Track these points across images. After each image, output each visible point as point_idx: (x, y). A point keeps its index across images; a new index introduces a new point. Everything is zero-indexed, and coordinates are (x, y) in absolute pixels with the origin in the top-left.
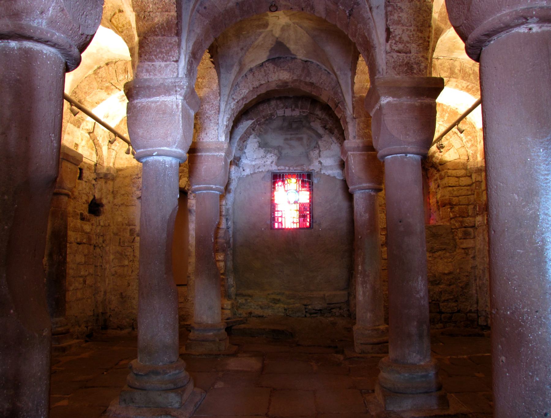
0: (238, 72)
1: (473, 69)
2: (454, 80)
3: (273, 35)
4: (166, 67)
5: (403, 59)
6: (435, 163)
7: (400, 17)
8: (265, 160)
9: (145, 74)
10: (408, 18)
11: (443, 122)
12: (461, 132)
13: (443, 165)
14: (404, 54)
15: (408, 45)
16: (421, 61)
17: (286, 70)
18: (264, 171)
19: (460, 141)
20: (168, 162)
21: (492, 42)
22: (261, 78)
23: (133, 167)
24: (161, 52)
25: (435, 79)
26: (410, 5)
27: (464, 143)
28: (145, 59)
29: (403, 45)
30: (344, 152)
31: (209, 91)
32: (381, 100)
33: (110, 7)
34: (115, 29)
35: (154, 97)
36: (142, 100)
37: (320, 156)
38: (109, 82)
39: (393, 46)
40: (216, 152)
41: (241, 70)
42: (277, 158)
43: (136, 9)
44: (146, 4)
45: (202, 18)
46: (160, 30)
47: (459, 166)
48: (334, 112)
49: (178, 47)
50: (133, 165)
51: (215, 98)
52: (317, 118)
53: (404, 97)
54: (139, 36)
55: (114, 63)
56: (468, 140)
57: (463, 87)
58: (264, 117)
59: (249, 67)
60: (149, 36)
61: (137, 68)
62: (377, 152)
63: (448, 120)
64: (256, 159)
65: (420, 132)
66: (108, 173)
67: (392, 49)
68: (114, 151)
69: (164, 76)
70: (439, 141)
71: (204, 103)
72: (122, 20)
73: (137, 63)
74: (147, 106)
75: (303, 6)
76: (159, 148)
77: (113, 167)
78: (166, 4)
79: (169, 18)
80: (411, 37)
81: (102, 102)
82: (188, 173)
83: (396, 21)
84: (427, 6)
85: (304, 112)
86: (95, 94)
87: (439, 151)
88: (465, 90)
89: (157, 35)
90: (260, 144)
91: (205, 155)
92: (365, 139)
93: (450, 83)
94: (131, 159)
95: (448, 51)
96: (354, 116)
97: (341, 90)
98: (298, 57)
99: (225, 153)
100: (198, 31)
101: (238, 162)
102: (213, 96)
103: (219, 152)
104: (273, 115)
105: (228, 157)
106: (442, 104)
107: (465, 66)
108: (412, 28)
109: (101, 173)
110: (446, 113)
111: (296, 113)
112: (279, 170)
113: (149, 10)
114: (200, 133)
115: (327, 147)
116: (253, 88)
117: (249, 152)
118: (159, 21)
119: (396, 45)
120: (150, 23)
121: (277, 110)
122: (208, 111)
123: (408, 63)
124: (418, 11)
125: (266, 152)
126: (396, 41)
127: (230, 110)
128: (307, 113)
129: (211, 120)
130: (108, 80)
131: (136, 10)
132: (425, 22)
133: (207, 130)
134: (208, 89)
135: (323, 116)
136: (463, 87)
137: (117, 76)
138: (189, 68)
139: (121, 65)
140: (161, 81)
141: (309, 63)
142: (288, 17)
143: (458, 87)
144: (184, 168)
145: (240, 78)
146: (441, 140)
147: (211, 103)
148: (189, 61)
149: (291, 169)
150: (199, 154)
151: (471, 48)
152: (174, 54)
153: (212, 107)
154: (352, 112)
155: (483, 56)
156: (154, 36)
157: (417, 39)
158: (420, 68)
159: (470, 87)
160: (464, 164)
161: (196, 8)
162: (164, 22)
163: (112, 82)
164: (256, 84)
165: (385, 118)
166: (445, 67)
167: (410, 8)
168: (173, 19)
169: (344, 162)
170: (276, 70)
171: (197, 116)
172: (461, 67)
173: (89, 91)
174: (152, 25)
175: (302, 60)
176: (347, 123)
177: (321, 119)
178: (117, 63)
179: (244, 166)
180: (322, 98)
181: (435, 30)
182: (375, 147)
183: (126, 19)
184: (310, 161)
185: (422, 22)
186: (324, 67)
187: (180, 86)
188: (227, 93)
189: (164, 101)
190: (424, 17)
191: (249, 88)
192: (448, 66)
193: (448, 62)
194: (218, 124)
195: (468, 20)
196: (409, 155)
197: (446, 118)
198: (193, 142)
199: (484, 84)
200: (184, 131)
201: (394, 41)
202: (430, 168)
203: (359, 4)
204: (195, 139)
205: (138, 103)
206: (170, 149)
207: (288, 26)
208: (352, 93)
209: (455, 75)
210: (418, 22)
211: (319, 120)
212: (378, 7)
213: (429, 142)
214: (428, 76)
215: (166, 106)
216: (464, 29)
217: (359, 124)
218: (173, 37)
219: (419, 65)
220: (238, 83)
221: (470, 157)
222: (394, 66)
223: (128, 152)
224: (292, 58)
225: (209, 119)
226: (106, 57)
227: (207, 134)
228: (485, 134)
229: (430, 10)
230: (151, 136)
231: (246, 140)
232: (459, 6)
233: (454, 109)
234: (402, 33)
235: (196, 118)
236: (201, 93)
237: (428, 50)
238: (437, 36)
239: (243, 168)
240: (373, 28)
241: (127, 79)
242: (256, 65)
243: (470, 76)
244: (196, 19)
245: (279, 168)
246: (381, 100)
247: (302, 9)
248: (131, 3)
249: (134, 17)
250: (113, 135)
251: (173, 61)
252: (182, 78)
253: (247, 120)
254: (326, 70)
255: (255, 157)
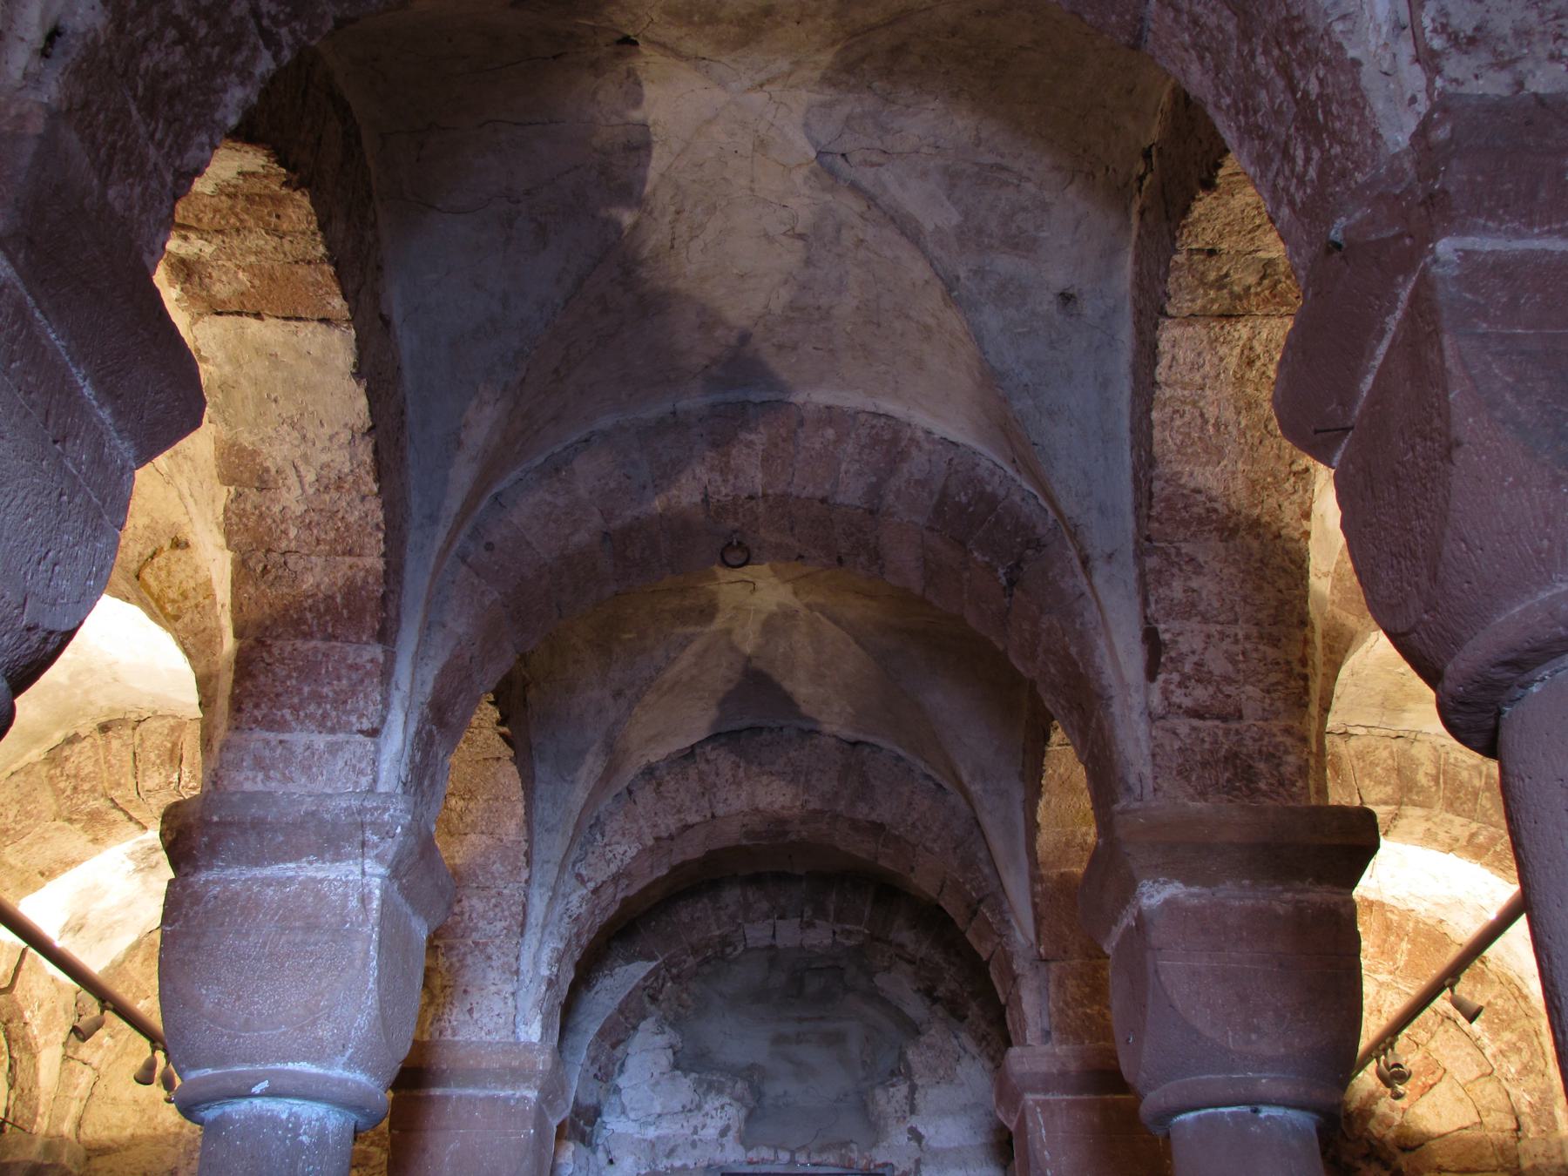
0: (601, 779)
1: (1485, 773)
2: (1419, 812)
3: (733, 648)
4: (330, 752)
5: (1216, 742)
6: (1381, 1140)
7: (1194, 591)
8: (696, 1120)
9: (250, 774)
10: (1224, 593)
11: (1391, 973)
12: (1472, 1016)
13: (1412, 1149)
14: (1217, 723)
15: (1228, 689)
16: (1282, 748)
17: (781, 775)
18: (692, 1166)
19: (1470, 1050)
20: (310, 1123)
21: (1535, 689)
22: (688, 803)
23: (156, 1140)
24: (318, 698)
25: (1342, 811)
26: (1227, 549)
27: (1492, 1062)
28: (256, 721)
29: (1211, 690)
30: (1007, 1091)
31: (488, 846)
32: (1143, 894)
33: (140, 526)
34: (153, 604)
35: (277, 863)
36: (230, 871)
37: (913, 1110)
38: (104, 795)
39: (1172, 692)
40: (504, 1084)
41: (611, 771)
42: (743, 1113)
43: (236, 539)
44: (274, 526)
45: (476, 582)
46: (320, 616)
47: (1482, 1157)
48: (963, 934)
49: (381, 683)
50: (160, 1131)
51: (511, 872)
52: (901, 958)
53: (1228, 883)
54: (238, 634)
55: (131, 725)
56: (1504, 1047)
57: (1457, 840)
58: (695, 951)
59: (644, 762)
60: (278, 637)
61: (221, 750)
62: (1139, 1098)
63: (1412, 969)
64: (659, 1116)
65: (1302, 1016)
66: (46, 1162)
67: (1169, 704)
68: (88, 1070)
69: (319, 786)
70: (1385, 1051)
71: (468, 892)
72: (183, 576)
73: (221, 733)
74: (244, 895)
75: (843, 551)
76: (279, 1066)
77: (73, 1138)
78: (347, 528)
79: (354, 576)
80: (1239, 662)
81: (64, 871)
82: (384, 1168)
83: (1180, 603)
84: (1287, 552)
85: (848, 934)
86: (43, 838)
87: (1389, 1091)
88: (1464, 848)
89: (308, 636)
90: (679, 1055)
91: (460, 1098)
92: (1087, 1042)
93: (1402, 823)
94: (155, 1103)
95: (1382, 705)
96: (1042, 951)
97: (988, 849)
98: (828, 728)
99: (541, 1090)
100: (459, 625)
101: (588, 1129)
102: (502, 865)
103: (514, 1085)
104: (730, 944)
105: (550, 1104)
106: (1382, 905)
107: (1452, 761)
108: (1240, 631)
109: (17, 1163)
110: (1402, 940)
111: (820, 937)
112: (750, 1163)
113: (284, 545)
114: (444, 1006)
115: (941, 1072)
116: (657, 839)
117: (632, 1087)
118: (318, 586)
119: (1183, 691)
120: (285, 590)
121: (746, 925)
122: (482, 924)
123: (1232, 757)
124: (1256, 569)
125: (700, 1091)
126: (1183, 675)
127: (567, 920)
128: (861, 938)
129: (489, 958)
130: (100, 788)
131: (237, 545)
132: (1287, 607)
133: (475, 997)
134: (484, 837)
135: (924, 950)
136: (1457, 840)
137: (140, 773)
138: (418, 759)
139: (156, 736)
140: (308, 805)
141: (867, 750)
142: (789, 587)
143: (1436, 840)
144: (373, 1149)
145: (609, 801)
146: (1391, 1045)
147: (494, 892)
148: (418, 733)
149: (801, 1158)
150: (437, 1092)
151: (1461, 708)
152: (366, 708)
153: (495, 906)
154: (1032, 936)
155: (1508, 736)
156: (296, 637)
157: (1262, 669)
158: (1280, 774)
159: (1481, 839)
160: (1502, 1149)
161: (457, 545)
162: (335, 588)
163: (114, 794)
164: (668, 827)
165: (1159, 963)
166: (1377, 765)
167: (1226, 561)
168: (371, 579)
169: (1010, 1133)
170: (741, 773)
171: (437, 942)
172: (1436, 763)
173: (19, 827)
174: (290, 598)
175: (841, 740)
176: (1015, 978)
177: (914, 963)
178: (143, 725)
179: (612, 1145)
180: (915, 881)
181: (1324, 637)
182: (1128, 1078)
183: (196, 571)
184: (874, 1129)
185: (1276, 608)
186: (922, 765)
187: (377, 827)
188: (558, 854)
189: (314, 880)
190: (1280, 591)
191: (639, 839)
192: (1390, 762)
193: (1386, 748)
194: (517, 972)
195: (1435, 609)
196: (1265, 1112)
197: (1402, 960)
198: (415, 1042)
199: (1525, 842)
200: (381, 1000)
201: (1176, 677)
202: (1360, 1164)
203: (1045, 546)
204: (422, 1032)
205: (215, 882)
206: (321, 1071)
207: (789, 615)
208: (1030, 864)
209: (1418, 793)
210: (1259, 610)
211: (909, 968)
212: (1110, 556)
213: (1345, 1062)
214: (1313, 802)
215: (320, 897)
216: (1427, 641)
217: (1060, 984)
218: (367, 643)
219: (1276, 761)
220: (598, 818)
221: (1527, 1121)
222: (1182, 765)
223: (145, 1077)
224: (801, 730)
225: (481, 951)
226: (103, 704)
227: (470, 1011)
228: (1560, 1037)
229: (1301, 567)
230: (252, 1014)
231: (622, 1037)
232: (1399, 563)
233: (1430, 922)
234: (1205, 649)
235: (432, 948)
236: (457, 853)
237: (1306, 706)
238: (1333, 657)
239: (608, 1152)
240: (1095, 628)
241: (177, 789)
242: (669, 755)
243: (1477, 799)
244: (453, 582)
245: (753, 1155)
246: (1143, 894)
247: (840, 561)
248: (221, 519)
249: (228, 568)
250: (93, 1007)
251: (361, 732)
252: (388, 795)
253: (629, 960)
254: (928, 777)
255: (658, 1109)
